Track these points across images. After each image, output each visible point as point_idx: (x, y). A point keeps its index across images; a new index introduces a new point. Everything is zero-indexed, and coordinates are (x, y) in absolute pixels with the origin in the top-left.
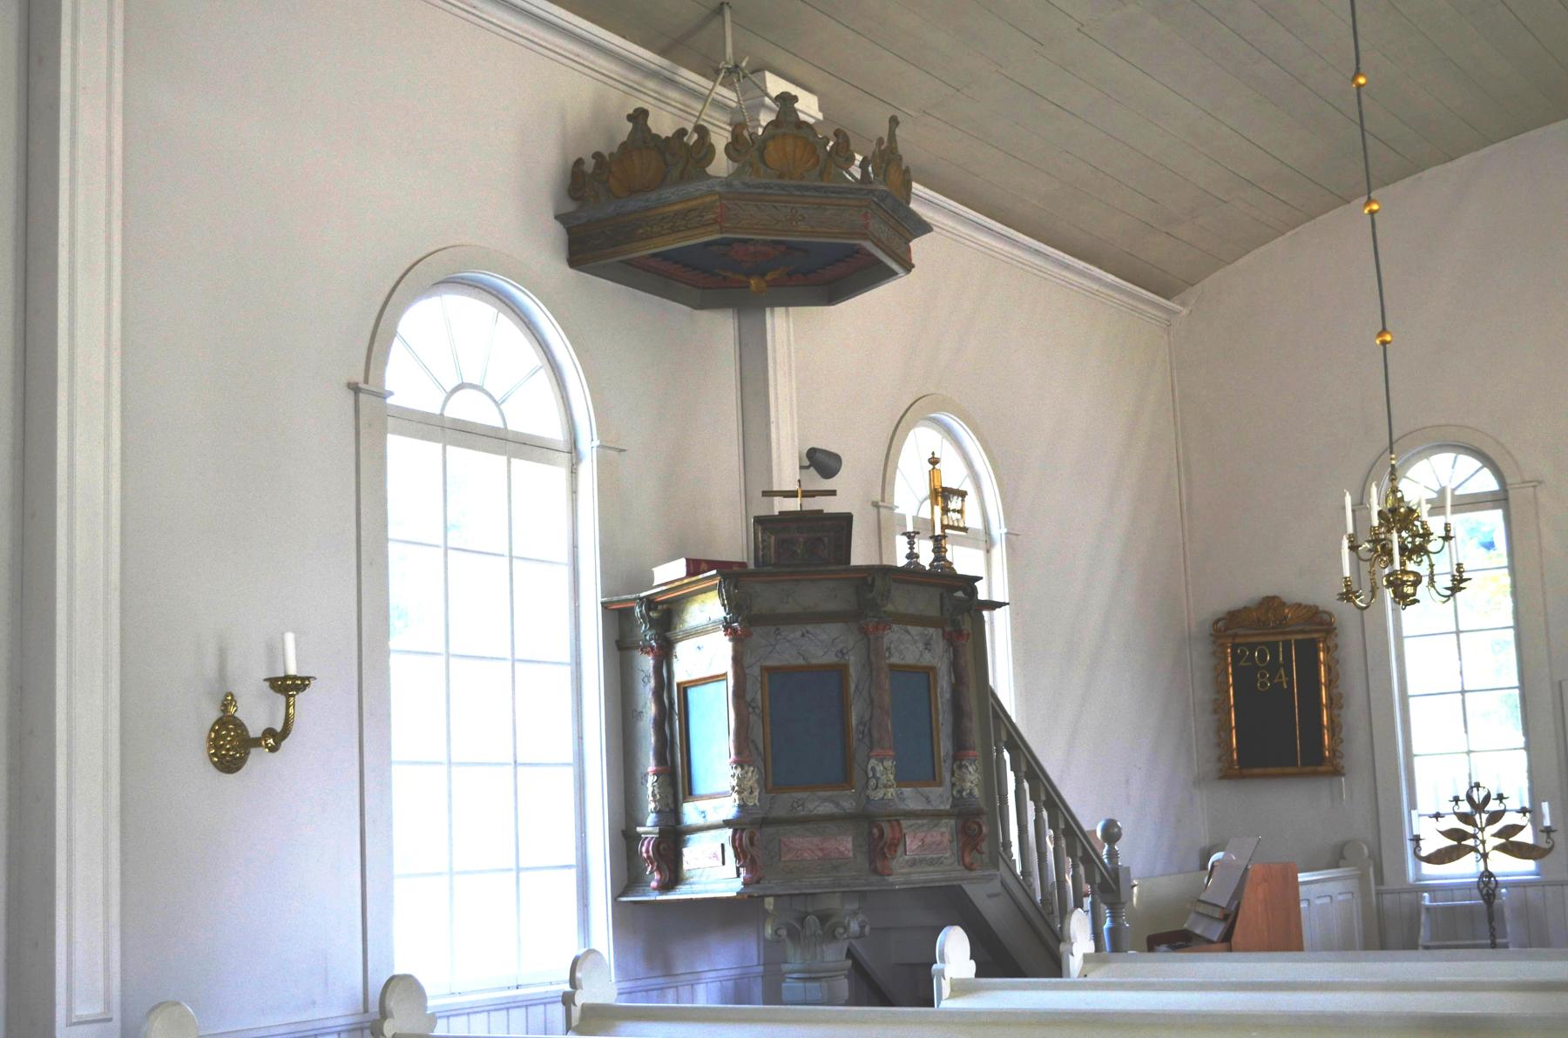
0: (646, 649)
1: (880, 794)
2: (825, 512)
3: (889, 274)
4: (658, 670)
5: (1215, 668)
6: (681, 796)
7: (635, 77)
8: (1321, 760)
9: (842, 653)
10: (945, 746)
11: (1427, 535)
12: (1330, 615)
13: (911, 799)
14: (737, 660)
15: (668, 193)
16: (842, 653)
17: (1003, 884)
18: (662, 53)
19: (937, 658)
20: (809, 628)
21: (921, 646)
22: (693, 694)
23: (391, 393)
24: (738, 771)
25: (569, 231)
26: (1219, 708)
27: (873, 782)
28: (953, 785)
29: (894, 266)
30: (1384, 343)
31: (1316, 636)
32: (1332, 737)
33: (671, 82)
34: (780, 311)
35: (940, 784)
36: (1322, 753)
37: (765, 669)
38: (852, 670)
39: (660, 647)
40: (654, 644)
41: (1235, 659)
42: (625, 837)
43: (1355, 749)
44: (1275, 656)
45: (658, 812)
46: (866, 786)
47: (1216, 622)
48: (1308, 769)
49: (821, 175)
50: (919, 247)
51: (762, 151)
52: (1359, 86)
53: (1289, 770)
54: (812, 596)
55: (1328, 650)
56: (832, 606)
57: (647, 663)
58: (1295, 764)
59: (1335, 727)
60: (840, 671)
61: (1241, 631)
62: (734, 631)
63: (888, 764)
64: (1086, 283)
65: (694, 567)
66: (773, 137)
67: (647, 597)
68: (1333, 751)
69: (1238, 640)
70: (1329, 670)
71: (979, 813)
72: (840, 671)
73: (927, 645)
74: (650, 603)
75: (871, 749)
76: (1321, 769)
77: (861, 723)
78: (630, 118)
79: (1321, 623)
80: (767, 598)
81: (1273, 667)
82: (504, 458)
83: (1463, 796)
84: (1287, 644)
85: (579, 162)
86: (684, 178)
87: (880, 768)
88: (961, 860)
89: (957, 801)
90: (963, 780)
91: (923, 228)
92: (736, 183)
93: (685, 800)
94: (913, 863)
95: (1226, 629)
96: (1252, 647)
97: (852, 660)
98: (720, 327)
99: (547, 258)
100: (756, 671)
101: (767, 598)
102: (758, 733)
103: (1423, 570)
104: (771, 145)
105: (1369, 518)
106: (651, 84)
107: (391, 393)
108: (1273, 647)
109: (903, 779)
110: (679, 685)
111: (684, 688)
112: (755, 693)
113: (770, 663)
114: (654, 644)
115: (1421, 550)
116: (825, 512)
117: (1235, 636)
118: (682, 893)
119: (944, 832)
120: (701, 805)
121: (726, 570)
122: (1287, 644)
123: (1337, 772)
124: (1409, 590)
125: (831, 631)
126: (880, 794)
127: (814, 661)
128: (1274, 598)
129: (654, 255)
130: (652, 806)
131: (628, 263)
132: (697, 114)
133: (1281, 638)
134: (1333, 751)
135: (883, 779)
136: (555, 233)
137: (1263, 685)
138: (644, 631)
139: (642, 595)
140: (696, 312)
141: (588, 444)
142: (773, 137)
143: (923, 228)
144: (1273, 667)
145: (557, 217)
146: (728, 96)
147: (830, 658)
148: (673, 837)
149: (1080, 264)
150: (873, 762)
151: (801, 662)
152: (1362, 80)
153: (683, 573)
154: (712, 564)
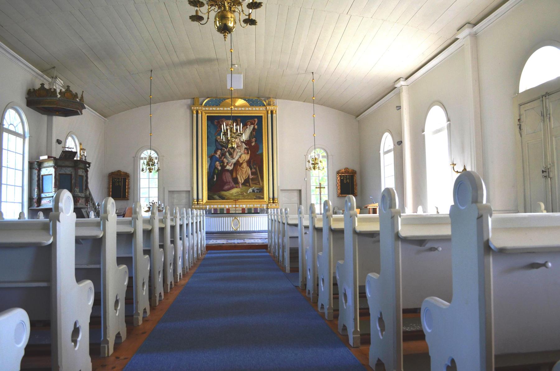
0: (36, 169)
1: (77, 193)
2: (453, 204)
3: (78, 114)
4: (38, 173)
5: (109, 181)
6: (41, 193)
7: (37, 75)
8: (126, 197)
9: (71, 172)
10: (84, 188)
11: (154, 163)
12: (129, 174)
13: (80, 194)
14: (55, 172)
15: (48, 98)
16: (71, 172)
17: (86, 211)
18: (41, 72)
19: (84, 174)
20: (66, 168)
21: (82, 172)
22: (44, 177)
23: (4, 125)
24: (55, 189)
25: (27, 100)
26: (109, 188)
27: (76, 192)
28: (85, 193)
29: (80, 114)
30: (151, 135)
31: (126, 177)
32: (127, 194)
33: (42, 77)
34: (55, 116)
35: (83, 193)
36: (126, 196)
37: (59, 174)
38: (73, 175)
39: (39, 169)
40: (38, 168)
41: (112, 179)
42: (30, 199)
43: (131, 197)
44: (119, 180)
45: (37, 195)
46: (74, 192)
47: (110, 173)
48: (124, 199)
49: (73, 99)
50: (83, 111)
51: (64, 94)
52: (151, 98)
53: (120, 199)
54: (67, 163)
55: (128, 180)
56: (71, 165)
57: (36, 172)
58: (121, 198)
59: (128, 192)
60: (71, 175)
61: (113, 176)
62: (55, 168)
63: (78, 189)
64: (94, 114)
65: (49, 157)
66: (66, 92)
67: (38, 161)
68: (127, 196)
69: (113, 177)
70: (128, 183)
71: (89, 198)
72: (71, 175)
73: (83, 172)
74: (38, 162)
75: (75, 187)
76: (125, 199)
77: (74, 183)
78: (41, 84)
79: (127, 175)
80: (60, 163)
81: (119, 182)
82: (449, 213)
83: (151, 202)
84: (121, 178)
85: (30, 89)
86: (51, 96)
87: (77, 190)
88: (86, 204)
89: (86, 196)
90: (86, 193)
91: (85, 108)
92: (61, 99)
93: (42, 193)
94: (80, 204)
95: (111, 175)
96: (115, 178)
97: (73, 173)
98: (45, 117)
99: (23, 102)
100: (58, 174)
101: (60, 163)
102: (57, 183)
103: (153, 168)
104: (66, 94)
105: (86, 153)
106: (39, 77)
107: (4, 125)
108: (119, 179)
109: (80, 192)
110: (42, 175)
111: (43, 176)
112: (57, 177)
113: (60, 173)
114: (38, 168)
115: (153, 165)
116: (453, 204)
117: (113, 176)
118: (41, 208)
119: (83, 200)
120: (45, 194)
121: (55, 159)
122: (121, 178)
123: (128, 199)
124: (151, 170)
125: (70, 169)
126: (77, 193)
127: (67, 173)
128: (120, 171)
129: (43, 107)
130: (36, 194)
131: (37, 107)
132: (272, 209)
133: (120, 177)
134: (127, 196)
135: (77, 191)
136: (25, 100)
137: (117, 185)
138: (36, 166)
139: (37, 161)
140: (43, 115)
141: (27, 135)
142: (66, 92)
143: (85, 108)
144: (119, 182)
145: (26, 98)
146: (50, 80)
147: (70, 173)
148: (40, 199)
149: (94, 111)
150: (76, 189)
151: (65, 173)
152: (151, 97)
153: (47, 158)
154: (52, 157)
